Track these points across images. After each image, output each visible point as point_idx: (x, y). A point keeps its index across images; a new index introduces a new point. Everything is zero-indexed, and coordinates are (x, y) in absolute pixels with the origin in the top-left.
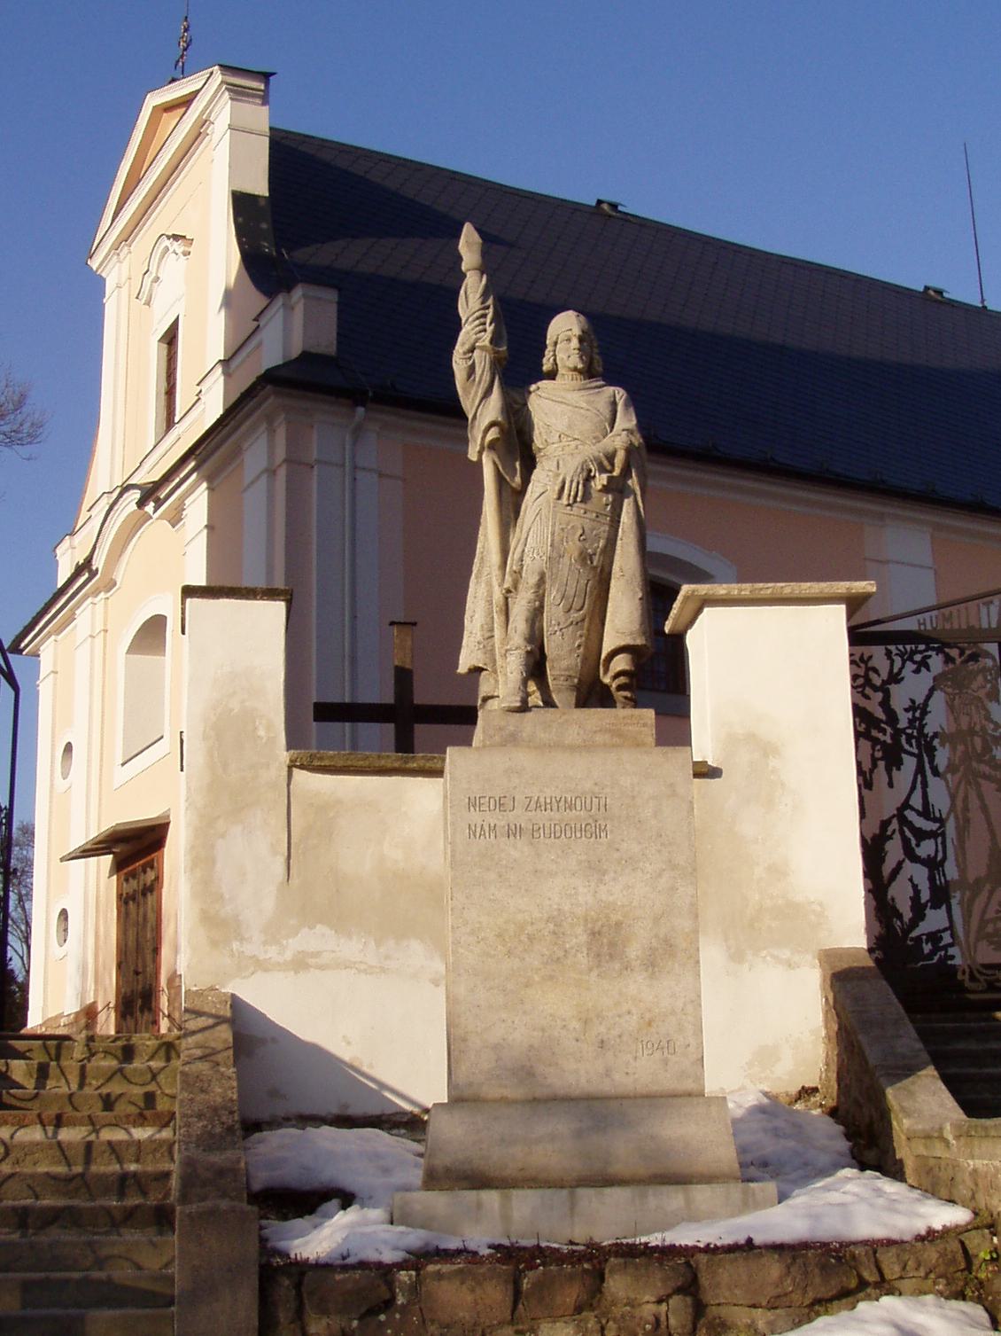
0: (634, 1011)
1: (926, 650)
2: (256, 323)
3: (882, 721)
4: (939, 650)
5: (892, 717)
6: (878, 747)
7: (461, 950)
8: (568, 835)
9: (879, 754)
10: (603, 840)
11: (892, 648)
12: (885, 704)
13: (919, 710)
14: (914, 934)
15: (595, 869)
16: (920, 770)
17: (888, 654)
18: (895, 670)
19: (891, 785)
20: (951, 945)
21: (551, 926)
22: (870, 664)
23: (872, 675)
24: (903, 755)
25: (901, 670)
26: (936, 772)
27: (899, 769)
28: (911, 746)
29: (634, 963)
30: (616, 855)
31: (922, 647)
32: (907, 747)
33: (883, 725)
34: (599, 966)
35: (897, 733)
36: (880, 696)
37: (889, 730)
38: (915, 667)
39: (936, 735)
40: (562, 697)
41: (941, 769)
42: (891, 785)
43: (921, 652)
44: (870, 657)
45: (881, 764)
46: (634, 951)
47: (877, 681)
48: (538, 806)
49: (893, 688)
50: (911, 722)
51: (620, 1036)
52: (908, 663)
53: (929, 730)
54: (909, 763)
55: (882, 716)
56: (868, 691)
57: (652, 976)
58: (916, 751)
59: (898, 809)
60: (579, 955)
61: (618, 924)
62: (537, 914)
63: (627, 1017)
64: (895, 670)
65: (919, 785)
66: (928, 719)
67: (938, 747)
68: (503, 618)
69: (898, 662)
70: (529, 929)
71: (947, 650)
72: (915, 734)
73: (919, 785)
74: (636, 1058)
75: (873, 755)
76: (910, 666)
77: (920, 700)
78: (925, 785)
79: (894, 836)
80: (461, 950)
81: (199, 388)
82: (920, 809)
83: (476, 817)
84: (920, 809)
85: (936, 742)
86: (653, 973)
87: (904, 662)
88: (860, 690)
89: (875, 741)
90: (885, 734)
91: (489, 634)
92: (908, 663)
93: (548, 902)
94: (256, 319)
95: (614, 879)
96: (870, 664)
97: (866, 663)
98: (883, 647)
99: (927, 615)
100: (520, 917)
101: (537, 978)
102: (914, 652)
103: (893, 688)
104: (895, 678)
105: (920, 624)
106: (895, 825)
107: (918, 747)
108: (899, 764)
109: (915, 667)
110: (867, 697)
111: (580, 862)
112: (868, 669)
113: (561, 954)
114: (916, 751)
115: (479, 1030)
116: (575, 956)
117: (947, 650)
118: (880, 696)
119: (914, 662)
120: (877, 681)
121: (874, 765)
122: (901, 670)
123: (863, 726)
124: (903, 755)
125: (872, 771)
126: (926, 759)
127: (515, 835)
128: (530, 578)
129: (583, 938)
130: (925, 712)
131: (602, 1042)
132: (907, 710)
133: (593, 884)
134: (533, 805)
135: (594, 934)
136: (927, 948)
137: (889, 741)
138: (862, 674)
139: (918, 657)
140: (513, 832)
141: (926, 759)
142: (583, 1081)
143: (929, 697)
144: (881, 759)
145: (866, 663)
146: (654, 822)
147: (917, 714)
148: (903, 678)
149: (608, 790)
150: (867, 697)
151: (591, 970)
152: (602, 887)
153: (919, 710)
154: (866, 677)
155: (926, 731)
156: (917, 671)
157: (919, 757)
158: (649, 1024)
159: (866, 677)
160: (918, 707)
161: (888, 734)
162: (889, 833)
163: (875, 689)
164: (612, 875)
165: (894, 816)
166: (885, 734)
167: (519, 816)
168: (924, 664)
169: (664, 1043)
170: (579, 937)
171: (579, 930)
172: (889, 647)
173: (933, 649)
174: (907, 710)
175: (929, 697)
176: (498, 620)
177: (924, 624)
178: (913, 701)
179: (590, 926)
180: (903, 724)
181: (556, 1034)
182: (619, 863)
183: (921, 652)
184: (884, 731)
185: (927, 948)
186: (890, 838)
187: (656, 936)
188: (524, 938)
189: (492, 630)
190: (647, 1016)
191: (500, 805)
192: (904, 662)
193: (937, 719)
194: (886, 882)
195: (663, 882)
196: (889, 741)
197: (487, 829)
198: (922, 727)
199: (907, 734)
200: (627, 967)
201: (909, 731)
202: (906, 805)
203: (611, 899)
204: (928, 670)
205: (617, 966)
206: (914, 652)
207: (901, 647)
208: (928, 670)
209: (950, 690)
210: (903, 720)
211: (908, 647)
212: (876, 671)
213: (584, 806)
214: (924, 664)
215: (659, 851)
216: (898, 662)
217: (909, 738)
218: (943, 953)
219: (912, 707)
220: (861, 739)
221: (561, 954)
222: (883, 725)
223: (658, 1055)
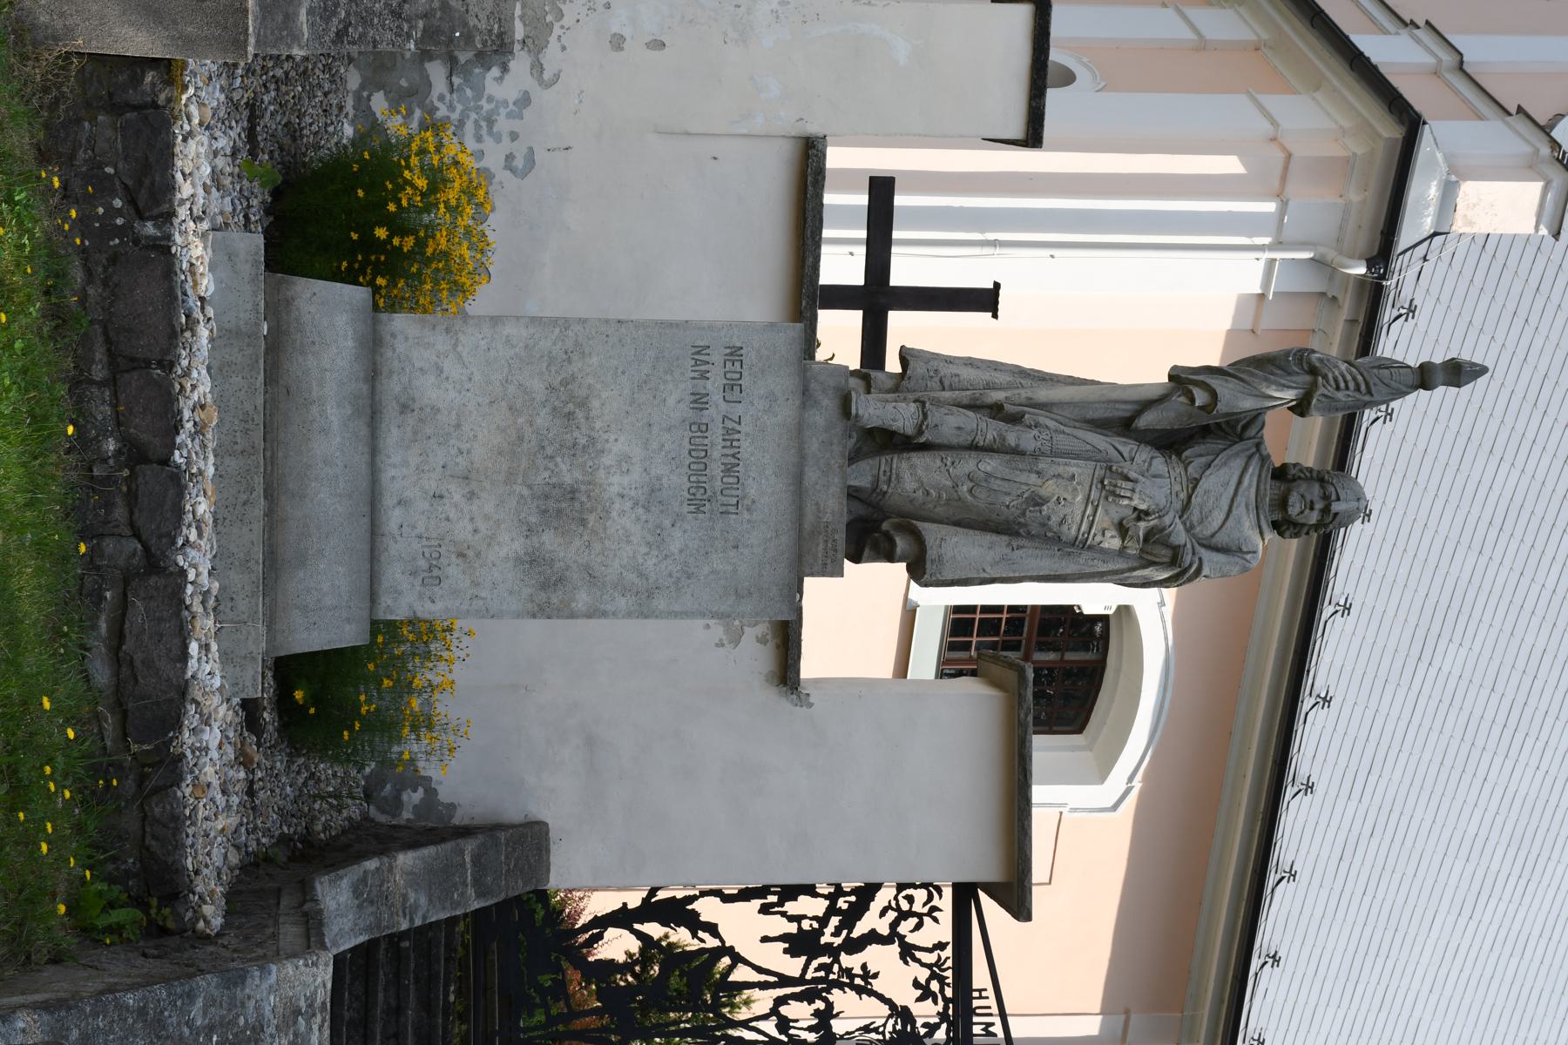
0: (477, 537)
1: (944, 998)
2: (1513, 110)
3: (850, 932)
4: (943, 1016)
5: (854, 946)
6: (816, 925)
7: (557, 330)
8: (694, 467)
9: (806, 925)
10: (686, 509)
11: (948, 952)
12: (873, 937)
13: (863, 984)
14: (565, 964)
15: (652, 496)
16: (784, 981)
17: (941, 946)
18: (918, 954)
19: (765, 939)
20: (547, 1013)
21: (583, 441)
22: (927, 919)
23: (913, 921)
24: (804, 958)
25: (918, 961)
26: (780, 1001)
27: (786, 951)
28: (817, 970)
29: (535, 539)
30: (667, 523)
31: (949, 992)
32: (815, 964)
33: (845, 932)
34: (533, 497)
35: (830, 950)
36: (884, 930)
37: (838, 941)
38: (923, 982)
39: (830, 1005)
40: (862, 475)
41: (784, 1010)
42: (765, 939)
43: (942, 991)
44: (936, 920)
45: (792, 928)
46: (549, 540)
47: (905, 927)
48: (728, 431)
49: (895, 948)
50: (848, 972)
51: (448, 519)
52: (927, 972)
53: (836, 996)
54: (793, 966)
55: (855, 934)
56: (892, 915)
57: (518, 560)
58: (808, 976)
59: (732, 948)
60: (546, 474)
61: (583, 522)
62: (598, 425)
63: (470, 528)
64: (918, 954)
65: (763, 978)
66: (851, 994)
67: (814, 1006)
68: (965, 401)
69: (930, 958)
70: (580, 415)
71: (944, 1026)
72: (832, 977)
73: (763, 978)
74: (420, 537)
75: (805, 917)
76: (923, 975)
77: (877, 985)
78: (764, 986)
79: (696, 941)
80: (557, 330)
81: (1421, 23)
82: (731, 978)
83: (717, 357)
84: (731, 978)
85: (820, 1005)
86: (522, 562)
87: (929, 966)
88: (893, 904)
89: (823, 921)
90: (833, 935)
91: (946, 383)
92: (927, 972)
93: (612, 438)
94: (1520, 110)
95: (638, 519)
96: (927, 919)
97: (929, 914)
98: (950, 939)
99: (992, 1002)
100: (595, 403)
101: (520, 421)
102: (942, 980)
103: (895, 948)
104: (908, 952)
105: (980, 991)
106: (715, 943)
107: (815, 980)
108: (792, 952)
109: (923, 982)
110: (883, 913)
111: (659, 479)
112: (920, 916)
113: (549, 451)
114: (808, 976)
115: (460, 348)
116: (546, 469)
117: (944, 1026)
118: (884, 930)
119: (928, 981)
120: (905, 927)
121: (791, 919)
122: (918, 961)
123: (845, 906)
124: (804, 958)
125: (783, 914)
126: (798, 989)
127: (695, 401)
128: (1013, 436)
129: (568, 479)
130: (860, 991)
131: (441, 497)
132: (864, 967)
133: (633, 493)
134: (730, 424)
135: (572, 493)
136: (546, 980)
137: (823, 940)
138: (914, 909)
139: (935, 986)
140: (699, 401)
141: (798, 989)
142: (392, 472)
143: (881, 998)
144: (800, 928)
145: (929, 914)
146: (706, 569)
147: (858, 981)
148: (906, 963)
149: (746, 516)
150: (883, 913)
151: (530, 487)
152: (629, 504)
153: (863, 984)
154: (910, 914)
155: (835, 991)
156: (916, 984)
157: (800, 981)
158: (461, 555)
159: (910, 914)
160: (867, 983)
161: (832, 940)
162: (701, 934)
163: (894, 925)
164: (644, 518)
165: (722, 941)
166: (833, 935)
167: (717, 407)
168: (926, 994)
169: (436, 572)
170: (568, 474)
171: (578, 475)
172: (950, 948)
173: (946, 1008)
174: (864, 967)
175: (881, 998)
176: (964, 396)
177: (981, 997)
178: (876, 976)
179: (583, 488)
180: (846, 960)
181: (452, 442)
182: (658, 527)
183: (942, 991)
184: (836, 934)
185: (546, 980)
186: (694, 935)
187: (568, 568)
188: (571, 406)
189: (952, 389)
190: (471, 553)
191: (730, 387)
192: (929, 966)
193: (852, 1012)
194: (637, 926)
195: (631, 577)
196: (823, 940)
197: (703, 368)
198: (841, 986)
199: (831, 965)
200: (530, 531)
201: (836, 968)
202: (737, 959)
203: (614, 514)
204: (918, 1000)
205: (533, 519)
206: (942, 980)
207: (949, 963)
208: (918, 1000)
209: (889, 1028)
210: (849, 961)
211: (949, 973)
212: (918, 926)
213: (729, 486)
214: (926, 994)
215: (670, 575)
216: (930, 958)
217: (826, 968)
218: (538, 1000)
219: (867, 975)
220: (827, 902)
221: (549, 451)
222: (845, 932)
223: (422, 563)
